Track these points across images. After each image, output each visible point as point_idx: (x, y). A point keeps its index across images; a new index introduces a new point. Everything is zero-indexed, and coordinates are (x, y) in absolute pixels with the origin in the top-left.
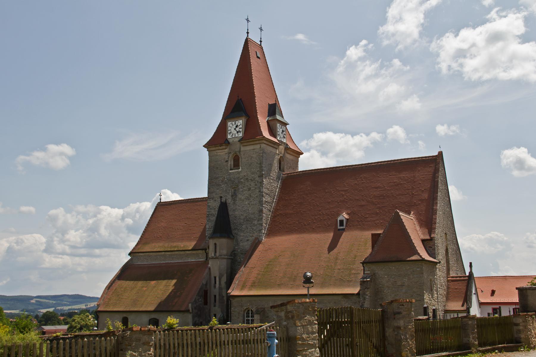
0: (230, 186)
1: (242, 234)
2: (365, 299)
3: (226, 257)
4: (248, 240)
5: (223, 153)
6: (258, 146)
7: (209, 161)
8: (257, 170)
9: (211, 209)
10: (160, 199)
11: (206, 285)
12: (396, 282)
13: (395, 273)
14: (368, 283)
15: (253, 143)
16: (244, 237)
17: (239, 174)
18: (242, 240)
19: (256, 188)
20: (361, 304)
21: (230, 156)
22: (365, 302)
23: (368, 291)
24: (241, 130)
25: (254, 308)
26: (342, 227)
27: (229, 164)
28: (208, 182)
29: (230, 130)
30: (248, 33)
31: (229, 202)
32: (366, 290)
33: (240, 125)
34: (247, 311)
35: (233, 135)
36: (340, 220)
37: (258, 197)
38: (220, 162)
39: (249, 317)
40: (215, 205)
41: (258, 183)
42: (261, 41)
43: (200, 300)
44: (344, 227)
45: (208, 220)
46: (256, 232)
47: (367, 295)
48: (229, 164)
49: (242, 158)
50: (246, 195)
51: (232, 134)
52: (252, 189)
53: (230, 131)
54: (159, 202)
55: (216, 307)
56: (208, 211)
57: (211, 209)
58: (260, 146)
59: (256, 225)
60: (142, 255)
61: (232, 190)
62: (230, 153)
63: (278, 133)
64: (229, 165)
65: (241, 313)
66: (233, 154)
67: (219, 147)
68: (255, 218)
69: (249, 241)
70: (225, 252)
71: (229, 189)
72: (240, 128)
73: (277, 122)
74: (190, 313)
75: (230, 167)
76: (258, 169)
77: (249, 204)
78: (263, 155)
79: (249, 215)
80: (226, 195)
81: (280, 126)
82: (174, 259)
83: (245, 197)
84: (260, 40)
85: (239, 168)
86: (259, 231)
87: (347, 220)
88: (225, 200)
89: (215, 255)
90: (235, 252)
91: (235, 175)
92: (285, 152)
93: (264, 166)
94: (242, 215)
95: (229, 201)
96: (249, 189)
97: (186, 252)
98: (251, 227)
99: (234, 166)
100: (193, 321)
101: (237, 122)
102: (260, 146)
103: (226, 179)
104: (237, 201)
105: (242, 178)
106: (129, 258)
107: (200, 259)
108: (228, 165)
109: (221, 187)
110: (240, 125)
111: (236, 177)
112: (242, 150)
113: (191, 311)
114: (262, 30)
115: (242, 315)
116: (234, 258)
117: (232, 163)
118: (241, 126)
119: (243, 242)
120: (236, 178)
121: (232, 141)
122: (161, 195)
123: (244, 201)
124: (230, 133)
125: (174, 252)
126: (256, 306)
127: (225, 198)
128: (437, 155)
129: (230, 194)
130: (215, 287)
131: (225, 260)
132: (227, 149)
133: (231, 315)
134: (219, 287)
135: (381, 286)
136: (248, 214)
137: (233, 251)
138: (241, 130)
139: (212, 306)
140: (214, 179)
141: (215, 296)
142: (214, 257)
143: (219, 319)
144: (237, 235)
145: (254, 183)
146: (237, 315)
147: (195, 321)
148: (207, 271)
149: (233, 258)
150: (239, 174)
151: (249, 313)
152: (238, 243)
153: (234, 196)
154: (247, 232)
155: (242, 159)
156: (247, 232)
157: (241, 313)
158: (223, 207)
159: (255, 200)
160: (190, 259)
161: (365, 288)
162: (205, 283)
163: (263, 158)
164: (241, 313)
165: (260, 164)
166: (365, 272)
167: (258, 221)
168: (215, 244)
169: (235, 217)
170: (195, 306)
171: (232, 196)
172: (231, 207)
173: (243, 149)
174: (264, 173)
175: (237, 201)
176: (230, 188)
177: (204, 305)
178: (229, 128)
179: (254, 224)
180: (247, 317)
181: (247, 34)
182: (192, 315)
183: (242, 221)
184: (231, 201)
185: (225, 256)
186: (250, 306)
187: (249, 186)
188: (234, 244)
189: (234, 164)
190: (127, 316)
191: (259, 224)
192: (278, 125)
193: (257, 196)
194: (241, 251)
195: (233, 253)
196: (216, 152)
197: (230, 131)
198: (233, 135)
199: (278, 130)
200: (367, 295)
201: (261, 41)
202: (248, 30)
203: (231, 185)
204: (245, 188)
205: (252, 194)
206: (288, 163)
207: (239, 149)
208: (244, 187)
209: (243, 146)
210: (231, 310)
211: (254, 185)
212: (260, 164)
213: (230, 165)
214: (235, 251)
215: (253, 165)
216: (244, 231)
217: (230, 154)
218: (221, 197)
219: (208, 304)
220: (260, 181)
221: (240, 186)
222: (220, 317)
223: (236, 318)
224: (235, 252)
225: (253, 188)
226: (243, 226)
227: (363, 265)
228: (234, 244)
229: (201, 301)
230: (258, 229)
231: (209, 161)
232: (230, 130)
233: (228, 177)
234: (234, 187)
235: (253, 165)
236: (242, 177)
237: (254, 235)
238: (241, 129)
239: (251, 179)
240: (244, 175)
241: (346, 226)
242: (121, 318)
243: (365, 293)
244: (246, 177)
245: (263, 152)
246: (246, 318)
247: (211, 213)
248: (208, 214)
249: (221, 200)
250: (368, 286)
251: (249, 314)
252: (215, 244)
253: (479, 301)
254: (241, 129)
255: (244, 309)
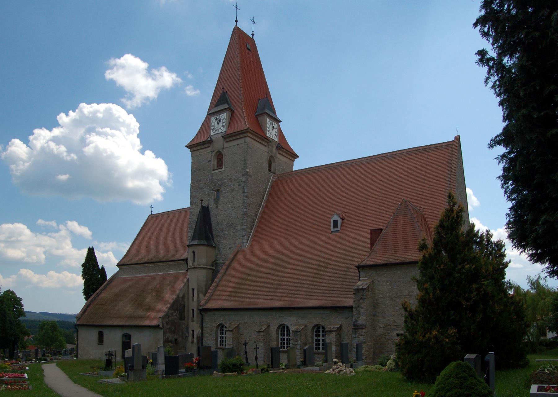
0: (212, 188)
1: (224, 242)
2: (359, 313)
3: (206, 267)
4: (230, 248)
5: (207, 154)
6: (242, 141)
7: (192, 163)
8: (241, 168)
9: (193, 215)
10: (152, 211)
11: (183, 297)
12: (402, 290)
13: (400, 279)
14: (365, 292)
15: (237, 137)
16: (226, 245)
17: (222, 174)
18: (224, 249)
19: (239, 189)
20: (354, 320)
21: (213, 155)
22: (359, 317)
23: (364, 303)
24: (224, 124)
25: (227, 324)
26: (336, 229)
27: (212, 164)
28: (191, 185)
29: (214, 126)
30: (236, 21)
31: (211, 207)
32: (361, 301)
33: (224, 119)
34: (221, 327)
35: (216, 131)
36: (333, 221)
37: (242, 198)
38: (202, 163)
39: (284, 336)
40: (197, 210)
41: (242, 182)
42: (253, 35)
43: (175, 314)
44: (339, 229)
45: (190, 228)
46: (239, 239)
47: (362, 308)
48: (212, 164)
49: (225, 156)
50: (229, 197)
51: (217, 130)
52: (235, 190)
53: (214, 127)
54: (151, 214)
55: (194, 323)
56: (191, 217)
57: (193, 215)
58: (245, 140)
59: (239, 230)
60: (127, 267)
61: (214, 193)
62: (213, 151)
63: (268, 129)
64: (212, 165)
65: (214, 330)
66: (216, 153)
67: (202, 146)
68: (238, 223)
69: (232, 249)
70: (204, 261)
71: (212, 191)
72: (223, 123)
73: (266, 117)
74: (161, 328)
75: (213, 167)
76: (242, 167)
77: (232, 207)
78: (247, 150)
79: (232, 219)
80: (209, 198)
81: (270, 122)
82: (157, 271)
83: (227, 200)
84: (252, 33)
85: (222, 168)
86: (242, 237)
87: (342, 221)
88: (207, 204)
89: (193, 264)
90: (217, 262)
91: (218, 176)
92: (277, 152)
93: (249, 163)
94: (224, 220)
95: (212, 206)
96: (233, 190)
97: (167, 263)
98: (233, 233)
99: (218, 166)
100: (163, 338)
101: (220, 116)
102: (245, 140)
103: (208, 181)
104: (219, 204)
105: (225, 179)
106: (118, 269)
107: (182, 270)
108: (211, 165)
109: (203, 190)
110: (224, 119)
111: (218, 178)
112: (225, 147)
113: (161, 326)
114: (254, 22)
115: (215, 332)
116: (216, 268)
117: (216, 163)
118: (224, 120)
119: (225, 250)
120: (219, 179)
121: (215, 138)
122: (153, 207)
123: (226, 204)
124: (213, 129)
125: (156, 264)
126: (230, 322)
127: (207, 202)
128: (454, 140)
129: (213, 197)
130: (193, 300)
131: (205, 271)
132: (210, 148)
133: (203, 331)
134: (197, 300)
135: (381, 296)
136: (231, 218)
137: (215, 261)
138: (224, 124)
139: (190, 320)
140: (197, 182)
141: (193, 310)
142: (192, 267)
143: (198, 335)
144: (219, 242)
145: (237, 183)
146: (209, 332)
147: (166, 337)
148: (184, 282)
149: (215, 268)
150: (222, 174)
151: (285, 330)
152: (220, 251)
153: (217, 200)
154: (229, 239)
155: (226, 157)
156: (229, 239)
157: (213, 329)
158: (205, 213)
159: (238, 202)
160: (171, 271)
161: (360, 299)
162: (182, 296)
163: (247, 153)
164: (213, 329)
165: (245, 160)
166: (361, 279)
167: (242, 225)
168: (194, 252)
169: (218, 223)
170: (167, 320)
171: (214, 199)
172: (213, 212)
173: (226, 145)
174: (248, 171)
175: (219, 204)
176: (213, 191)
177: (180, 320)
178: (213, 124)
179: (237, 230)
180: (220, 334)
181: (235, 23)
182: (163, 330)
183: (225, 227)
184: (214, 205)
185: (204, 265)
186: (223, 322)
187: (232, 186)
188: (216, 253)
189: (217, 164)
190: (102, 331)
191: (242, 229)
192: (268, 120)
193: (241, 198)
194: (223, 260)
195: (215, 262)
196: (199, 152)
197: (214, 127)
198: (216, 131)
199: (268, 126)
200: (362, 308)
201: (253, 35)
202: (236, 18)
203: (214, 187)
204: (228, 190)
205: (235, 196)
206: (280, 165)
207: (222, 146)
208: (227, 188)
209: (227, 142)
210: (203, 326)
211: (237, 185)
212: (245, 160)
213: (213, 165)
214: (217, 261)
215: (237, 163)
216: (226, 237)
217: (213, 153)
218: (202, 200)
219: (186, 319)
220: (244, 180)
221: (223, 188)
222: (198, 333)
223: (208, 335)
224: (217, 262)
225: (237, 189)
226: (225, 233)
227: (358, 269)
228: (216, 253)
229: (176, 315)
230: (241, 235)
231: (192, 162)
232: (214, 126)
233: (211, 178)
234: (216, 189)
235: (237, 163)
236: (225, 178)
237: (237, 242)
238: (225, 124)
239: (234, 179)
240: (227, 175)
241: (341, 227)
242: (98, 332)
243: (360, 305)
244: (230, 177)
245: (248, 146)
246: (219, 336)
247: (193, 220)
248: (190, 221)
249: (202, 203)
250: (364, 296)
251: (320, 332)
252: (194, 252)
253: (101, 368)
254: (225, 124)
255: (217, 325)
